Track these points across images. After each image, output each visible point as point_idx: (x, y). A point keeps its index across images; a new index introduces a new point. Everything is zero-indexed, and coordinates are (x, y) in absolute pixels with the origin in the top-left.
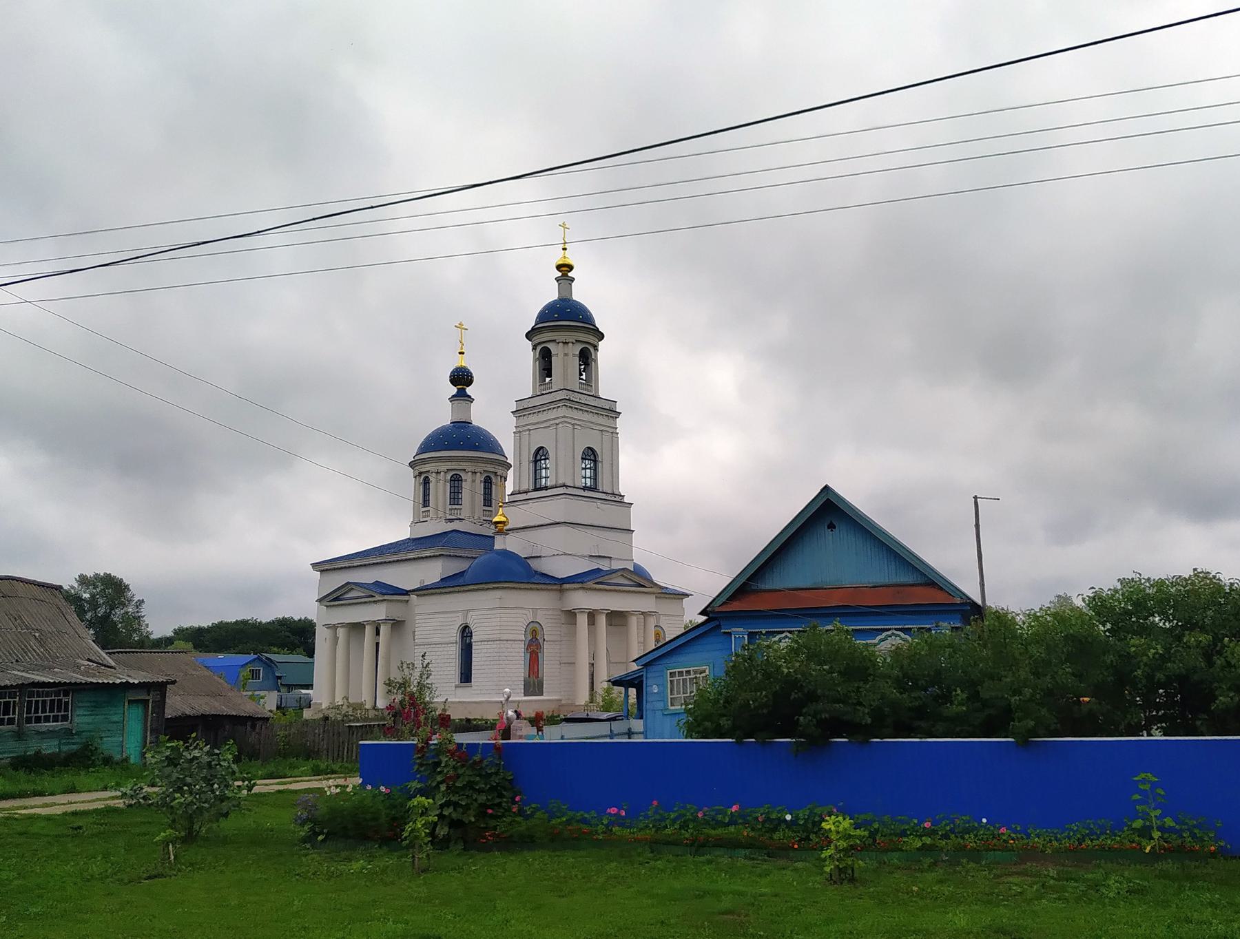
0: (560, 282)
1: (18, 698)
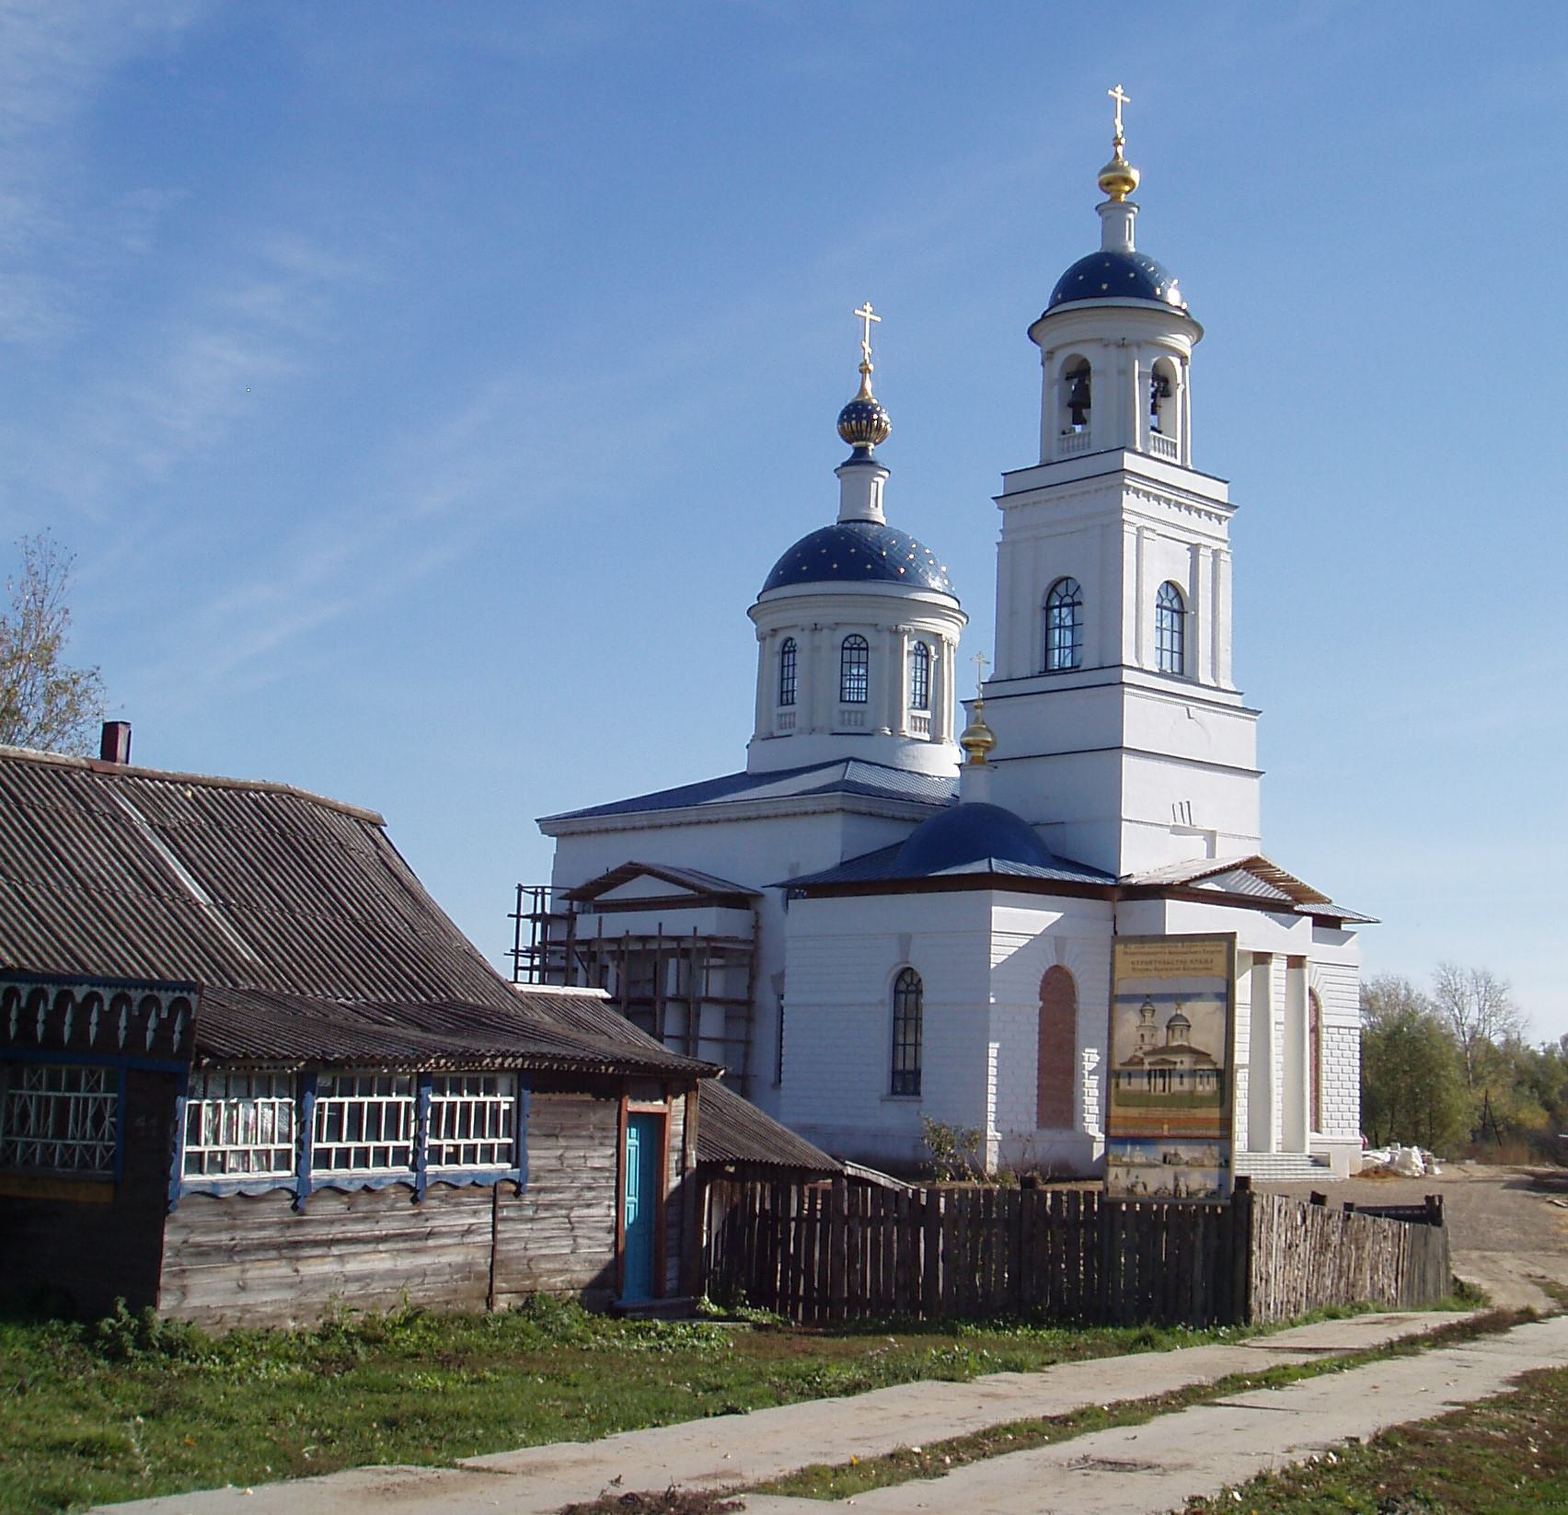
0: (1106, 214)
1: (219, 1101)
